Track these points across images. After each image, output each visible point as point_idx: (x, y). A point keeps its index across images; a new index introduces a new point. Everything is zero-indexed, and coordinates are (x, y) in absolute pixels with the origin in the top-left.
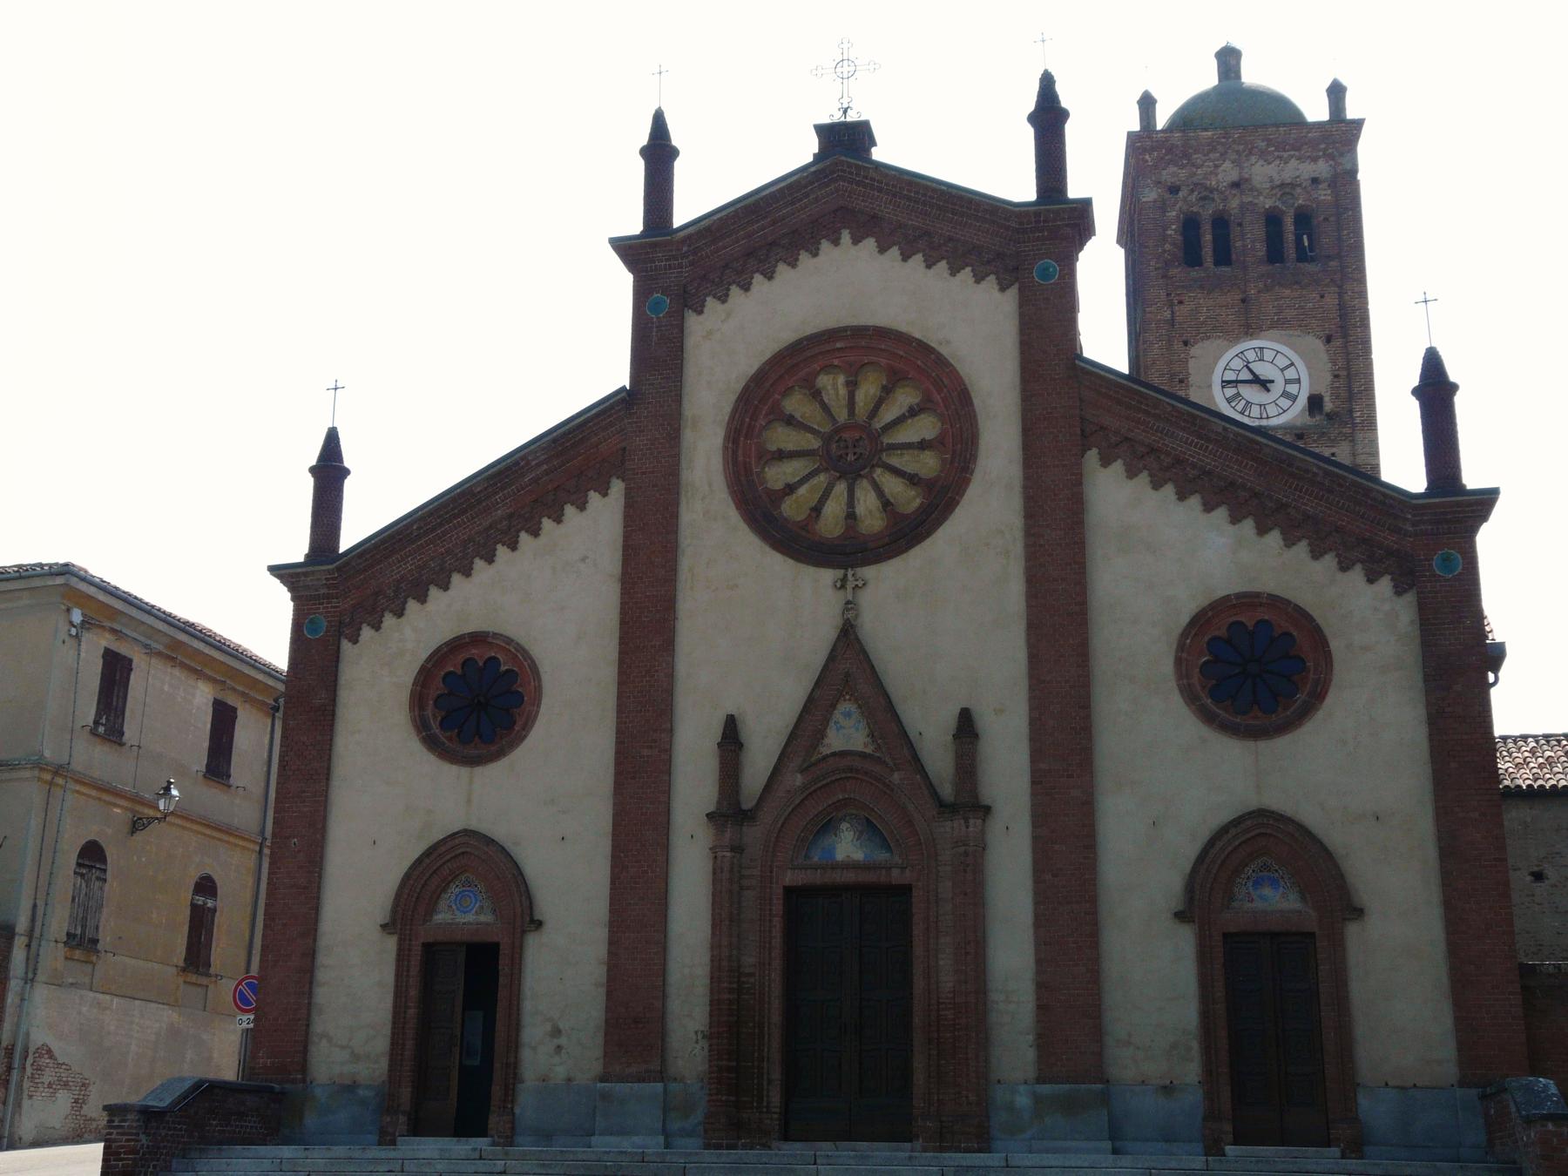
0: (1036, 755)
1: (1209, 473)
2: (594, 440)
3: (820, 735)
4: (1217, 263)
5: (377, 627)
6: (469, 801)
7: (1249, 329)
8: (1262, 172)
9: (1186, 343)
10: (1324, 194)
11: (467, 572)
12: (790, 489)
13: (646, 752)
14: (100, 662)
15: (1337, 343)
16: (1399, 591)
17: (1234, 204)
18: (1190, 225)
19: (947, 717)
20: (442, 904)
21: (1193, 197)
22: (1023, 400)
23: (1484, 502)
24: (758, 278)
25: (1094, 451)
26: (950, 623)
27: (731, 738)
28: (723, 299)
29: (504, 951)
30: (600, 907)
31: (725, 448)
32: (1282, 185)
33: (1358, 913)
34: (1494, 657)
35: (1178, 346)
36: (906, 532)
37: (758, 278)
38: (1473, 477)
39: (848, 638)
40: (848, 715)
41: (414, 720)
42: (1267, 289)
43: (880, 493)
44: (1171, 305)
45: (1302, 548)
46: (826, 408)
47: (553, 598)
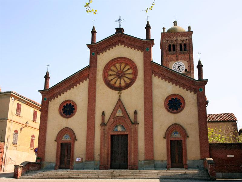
0: (145, 116)
1: (169, 78)
2: (85, 73)
3: (115, 114)
4: (173, 51)
5: (54, 99)
6: (67, 123)
7: (177, 60)
8: (179, 39)
9: (169, 62)
10: (187, 42)
11: (67, 91)
12: (112, 80)
13: (91, 116)
14: (17, 105)
15: (189, 62)
16: (194, 94)
17: (175, 43)
18: (170, 46)
19: (133, 111)
20: (63, 137)
21: (170, 42)
22: (144, 67)
23: (206, 81)
24: (107, 50)
25: (153, 75)
26: (133, 98)
27: (103, 114)
28: (102, 53)
29: (72, 144)
30: (85, 138)
31: (103, 74)
32: (182, 40)
33: (188, 137)
34: (207, 102)
35: (168, 62)
36: (128, 86)
37: (107, 50)
38: (205, 78)
39: (119, 100)
40: (119, 111)
41: (59, 112)
42: (180, 55)
43: (124, 80)
44: (167, 57)
45: (182, 88)
46: (117, 68)
47: (78, 95)
